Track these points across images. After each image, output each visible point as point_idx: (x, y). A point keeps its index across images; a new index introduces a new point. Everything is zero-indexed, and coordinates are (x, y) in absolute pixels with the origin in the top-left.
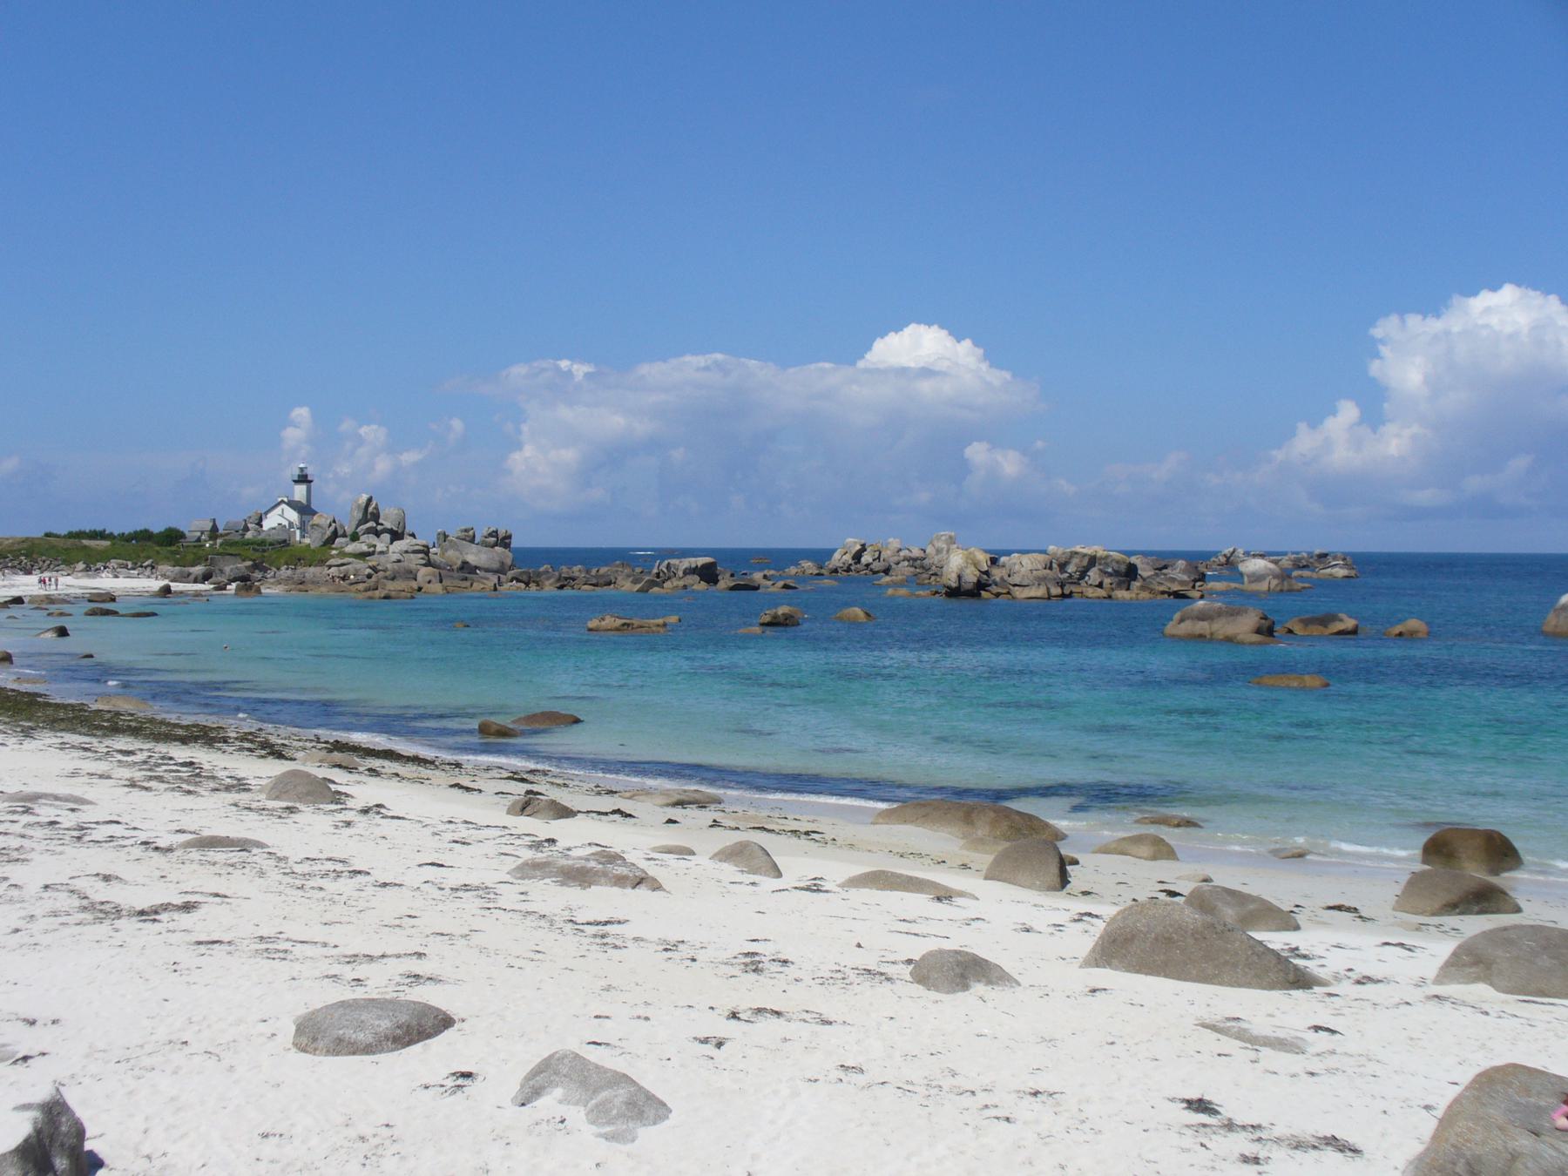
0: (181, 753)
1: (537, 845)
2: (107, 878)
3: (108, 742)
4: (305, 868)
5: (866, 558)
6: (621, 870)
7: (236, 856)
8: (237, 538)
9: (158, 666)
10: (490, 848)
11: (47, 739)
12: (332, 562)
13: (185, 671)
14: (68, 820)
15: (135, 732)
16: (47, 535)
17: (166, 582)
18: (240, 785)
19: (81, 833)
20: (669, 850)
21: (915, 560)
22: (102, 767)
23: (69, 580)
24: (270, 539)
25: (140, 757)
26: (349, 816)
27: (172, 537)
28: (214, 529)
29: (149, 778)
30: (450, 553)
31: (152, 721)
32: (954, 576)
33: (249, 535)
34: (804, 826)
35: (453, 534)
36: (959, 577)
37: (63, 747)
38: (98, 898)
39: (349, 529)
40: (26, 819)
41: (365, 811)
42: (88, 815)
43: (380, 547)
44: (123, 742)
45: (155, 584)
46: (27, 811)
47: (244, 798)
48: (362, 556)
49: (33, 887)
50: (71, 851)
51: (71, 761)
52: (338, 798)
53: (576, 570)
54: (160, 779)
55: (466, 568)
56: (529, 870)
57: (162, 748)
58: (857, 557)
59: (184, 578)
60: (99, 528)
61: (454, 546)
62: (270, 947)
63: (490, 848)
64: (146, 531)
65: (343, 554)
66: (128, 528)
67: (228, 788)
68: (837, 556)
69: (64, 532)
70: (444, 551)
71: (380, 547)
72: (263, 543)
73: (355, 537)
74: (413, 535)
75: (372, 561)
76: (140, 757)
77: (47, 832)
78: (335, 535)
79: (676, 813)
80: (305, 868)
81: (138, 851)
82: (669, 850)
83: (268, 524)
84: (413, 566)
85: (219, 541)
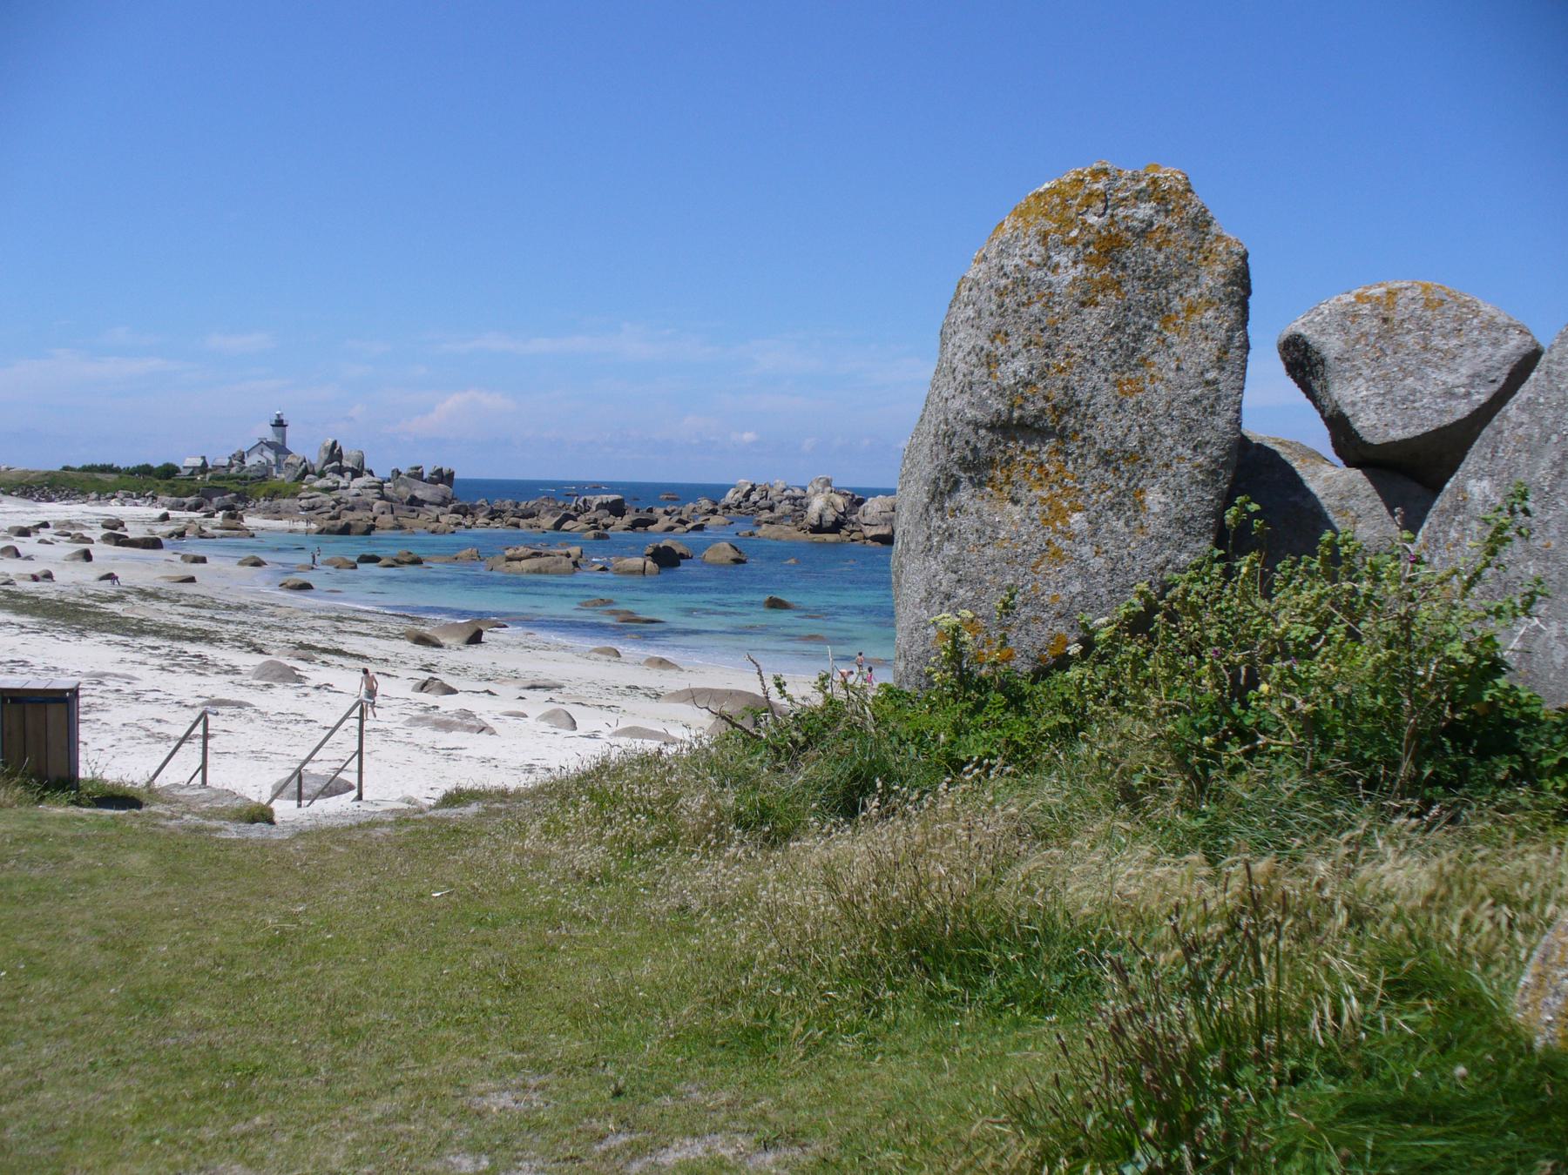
0: (192, 649)
1: (427, 709)
2: (159, 721)
3: (139, 640)
4: (278, 718)
5: (754, 497)
6: (471, 722)
7: (235, 711)
8: (223, 473)
9: (695, 627)
10: (395, 710)
11: (95, 638)
12: (302, 495)
13: (596, 588)
14: (127, 689)
15: (157, 633)
16: (66, 468)
17: (164, 510)
18: (234, 670)
19: (137, 696)
20: (510, 714)
21: (795, 499)
22: (139, 657)
23: (84, 507)
24: (251, 475)
25: (163, 651)
26: (305, 690)
27: (169, 471)
28: (205, 464)
29: (174, 663)
30: (402, 489)
31: (165, 625)
32: (816, 516)
33: (233, 471)
34: (607, 703)
35: (404, 470)
36: (821, 517)
37: (109, 643)
38: (156, 730)
39: (317, 469)
40: (100, 688)
41: (317, 688)
42: (139, 686)
43: (343, 483)
44: (149, 641)
45: (158, 512)
46: (100, 683)
47: (237, 678)
48: (328, 490)
49: (116, 725)
50: (134, 706)
51: (116, 653)
52: (300, 679)
53: (508, 504)
54: (179, 665)
55: (414, 502)
56: (415, 721)
57: (178, 645)
58: (747, 495)
59: (180, 507)
60: (108, 463)
61: (404, 482)
62: (257, 755)
63: (395, 710)
64: (147, 466)
65: (312, 489)
66: (133, 463)
67: (226, 672)
68: (730, 494)
69: (78, 466)
70: (397, 486)
71: (343, 483)
72: (245, 478)
73: (322, 475)
74: (371, 473)
75: (336, 495)
76: (163, 651)
77: (115, 695)
78: (306, 472)
79: (525, 693)
80: (278, 718)
81: (175, 707)
82: (510, 714)
83: (249, 462)
84: (369, 500)
85: (208, 475)
